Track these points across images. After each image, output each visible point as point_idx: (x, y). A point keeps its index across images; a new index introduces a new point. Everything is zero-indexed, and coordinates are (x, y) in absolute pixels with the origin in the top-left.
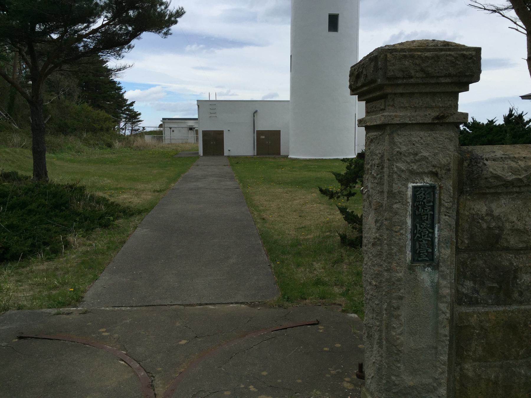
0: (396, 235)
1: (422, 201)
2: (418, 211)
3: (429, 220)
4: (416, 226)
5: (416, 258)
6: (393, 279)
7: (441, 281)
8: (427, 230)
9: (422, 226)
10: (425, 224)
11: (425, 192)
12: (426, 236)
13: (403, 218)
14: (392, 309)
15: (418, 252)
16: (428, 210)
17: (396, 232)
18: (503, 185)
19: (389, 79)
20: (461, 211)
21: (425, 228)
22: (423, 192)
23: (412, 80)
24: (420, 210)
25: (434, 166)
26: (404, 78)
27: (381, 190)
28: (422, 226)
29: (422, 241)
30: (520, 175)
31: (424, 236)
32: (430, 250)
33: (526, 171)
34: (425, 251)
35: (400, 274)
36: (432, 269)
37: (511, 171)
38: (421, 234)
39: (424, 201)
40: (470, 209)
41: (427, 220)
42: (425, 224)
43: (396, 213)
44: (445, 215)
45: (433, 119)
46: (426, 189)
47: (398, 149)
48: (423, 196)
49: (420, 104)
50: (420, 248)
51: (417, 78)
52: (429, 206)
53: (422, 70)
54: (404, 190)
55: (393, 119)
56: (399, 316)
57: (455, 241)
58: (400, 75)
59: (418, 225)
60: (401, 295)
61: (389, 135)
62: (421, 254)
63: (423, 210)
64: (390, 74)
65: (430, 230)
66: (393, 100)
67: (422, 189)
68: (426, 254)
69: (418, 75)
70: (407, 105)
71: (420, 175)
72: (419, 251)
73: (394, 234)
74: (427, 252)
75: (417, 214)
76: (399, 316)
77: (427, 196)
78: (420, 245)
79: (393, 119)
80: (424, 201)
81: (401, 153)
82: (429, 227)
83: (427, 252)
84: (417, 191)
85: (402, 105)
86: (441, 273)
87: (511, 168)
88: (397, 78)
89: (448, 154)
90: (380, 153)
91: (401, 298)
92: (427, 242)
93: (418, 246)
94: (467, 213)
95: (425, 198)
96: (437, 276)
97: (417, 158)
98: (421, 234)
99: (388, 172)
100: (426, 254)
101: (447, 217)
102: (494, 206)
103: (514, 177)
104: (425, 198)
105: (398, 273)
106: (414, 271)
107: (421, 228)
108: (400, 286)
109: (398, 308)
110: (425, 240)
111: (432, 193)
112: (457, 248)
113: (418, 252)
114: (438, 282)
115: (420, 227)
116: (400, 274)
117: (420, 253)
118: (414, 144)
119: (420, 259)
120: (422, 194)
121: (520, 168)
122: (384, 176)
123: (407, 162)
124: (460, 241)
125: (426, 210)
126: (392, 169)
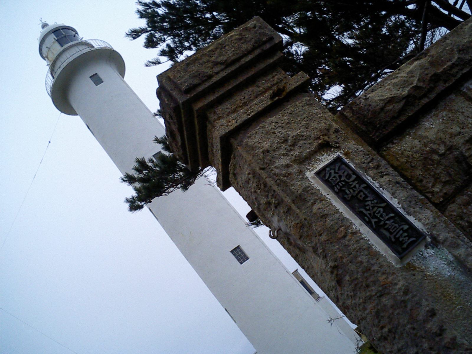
0: (349, 240)
1: (340, 181)
2: (347, 194)
3: (368, 195)
4: (361, 212)
5: (400, 249)
6: (399, 298)
7: (457, 253)
8: (379, 207)
9: (367, 208)
10: (369, 203)
11: (334, 169)
12: (384, 214)
13: (337, 216)
14: (437, 339)
15: (393, 240)
16: (357, 186)
17: (345, 236)
18: (405, 105)
19: (188, 91)
20: (395, 163)
21: (373, 207)
22: (332, 171)
23: (215, 79)
24: (347, 192)
25: (318, 138)
26: (203, 82)
27: (285, 210)
28: (367, 208)
29: (385, 224)
30: (412, 84)
31: (381, 216)
32: (406, 227)
33: (413, 76)
34: (401, 232)
35: (401, 283)
36: (433, 248)
37: (399, 87)
38: (375, 217)
39: (342, 179)
40: (402, 154)
41: (367, 196)
42: (369, 203)
43: (324, 216)
44: (382, 177)
45: (272, 98)
46: (332, 167)
47: (261, 150)
48: (337, 175)
49: (247, 97)
50: (391, 233)
51: (217, 73)
52: (353, 181)
53: (216, 64)
54: (307, 184)
55: (227, 126)
56: (454, 339)
57: (423, 197)
58: (196, 81)
59: (362, 210)
60: (427, 309)
61: (240, 145)
62: (401, 239)
63: (351, 191)
64: (184, 87)
65: (383, 205)
66: (215, 112)
67: (327, 169)
68: (406, 234)
69: (216, 70)
70: (233, 107)
71: (310, 158)
72: (395, 237)
73: (345, 241)
74: (405, 231)
75: (348, 199)
76: (454, 339)
77: (341, 173)
78: (388, 230)
79: (227, 126)
80: (342, 179)
81: (268, 151)
82: (377, 203)
83: (405, 231)
84: (325, 176)
85: (228, 110)
86: (447, 244)
87: (395, 85)
88: (195, 86)
89: (320, 118)
90: (249, 174)
91: (432, 313)
92: (392, 221)
93: (387, 234)
94: (404, 160)
95: (340, 177)
96: (446, 252)
97: (290, 142)
98: (376, 217)
99: (273, 182)
100: (406, 234)
101: (385, 177)
102: (421, 132)
103: (407, 89)
104: (340, 177)
105: (396, 284)
106: (415, 268)
107: (369, 210)
108: (416, 299)
109: (442, 331)
110: (389, 219)
111: (343, 166)
112: (436, 205)
113: (393, 240)
114: (456, 257)
115: (367, 210)
116: (401, 283)
117: (397, 239)
118: (273, 133)
119: (405, 246)
120: (333, 175)
121: (405, 79)
122: (274, 191)
123: (283, 155)
124: (430, 195)
125: (355, 187)
126: (275, 174)
